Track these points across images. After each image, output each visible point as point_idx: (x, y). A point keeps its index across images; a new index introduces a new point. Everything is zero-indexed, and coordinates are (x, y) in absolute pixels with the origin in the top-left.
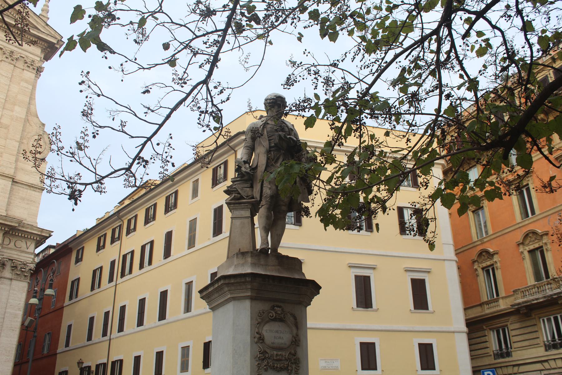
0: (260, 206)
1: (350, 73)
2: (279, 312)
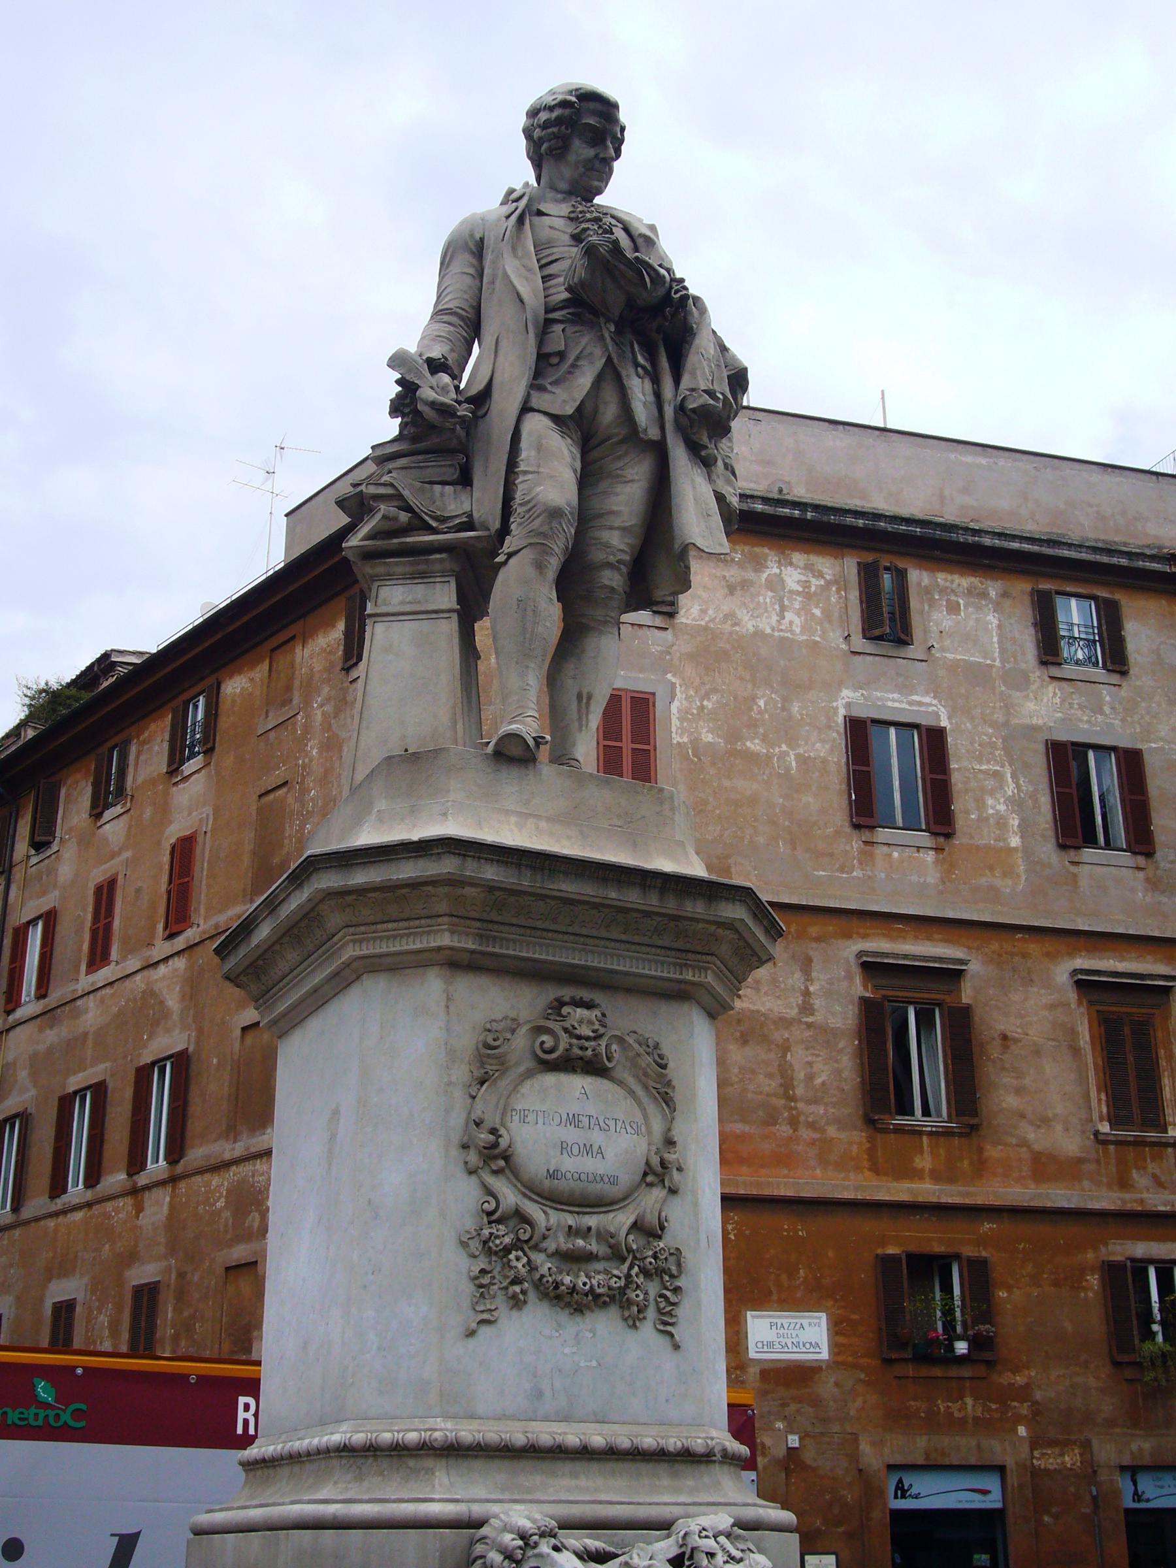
2: (585, 1031)
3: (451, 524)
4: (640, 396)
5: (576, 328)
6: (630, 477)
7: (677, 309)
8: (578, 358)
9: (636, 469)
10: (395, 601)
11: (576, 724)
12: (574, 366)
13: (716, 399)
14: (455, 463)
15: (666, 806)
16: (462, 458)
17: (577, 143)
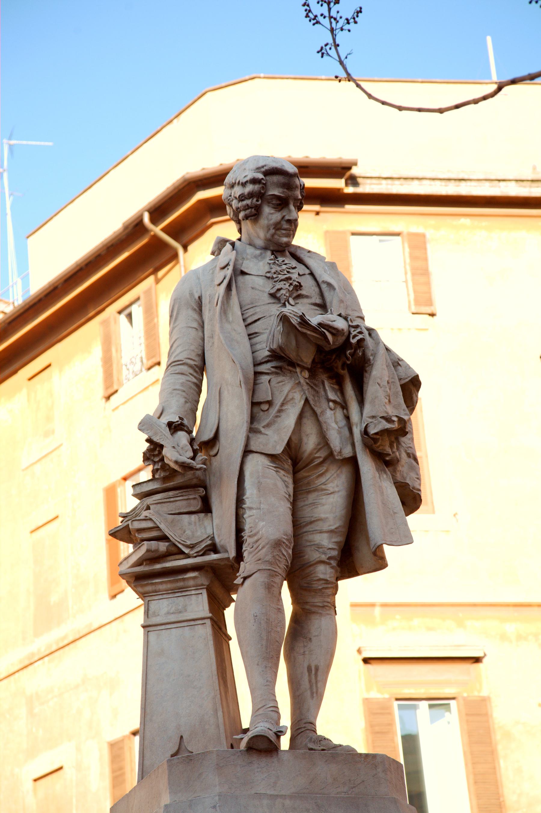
0: (238, 581)
1: (476, 102)
3: (199, 549)
4: (334, 425)
5: (280, 378)
6: (332, 490)
7: (356, 350)
8: (282, 405)
9: (336, 482)
10: (165, 610)
11: (308, 693)
12: (280, 411)
13: (392, 422)
14: (197, 496)
15: (380, 770)
16: (202, 491)
17: (267, 210)
